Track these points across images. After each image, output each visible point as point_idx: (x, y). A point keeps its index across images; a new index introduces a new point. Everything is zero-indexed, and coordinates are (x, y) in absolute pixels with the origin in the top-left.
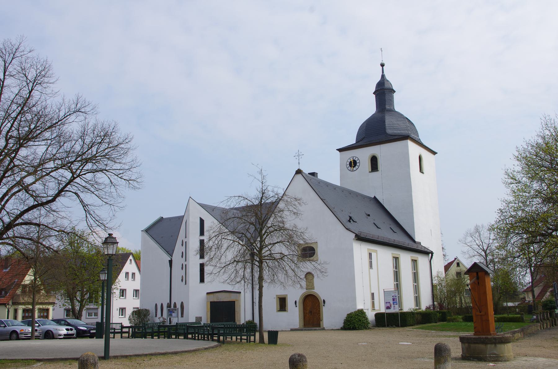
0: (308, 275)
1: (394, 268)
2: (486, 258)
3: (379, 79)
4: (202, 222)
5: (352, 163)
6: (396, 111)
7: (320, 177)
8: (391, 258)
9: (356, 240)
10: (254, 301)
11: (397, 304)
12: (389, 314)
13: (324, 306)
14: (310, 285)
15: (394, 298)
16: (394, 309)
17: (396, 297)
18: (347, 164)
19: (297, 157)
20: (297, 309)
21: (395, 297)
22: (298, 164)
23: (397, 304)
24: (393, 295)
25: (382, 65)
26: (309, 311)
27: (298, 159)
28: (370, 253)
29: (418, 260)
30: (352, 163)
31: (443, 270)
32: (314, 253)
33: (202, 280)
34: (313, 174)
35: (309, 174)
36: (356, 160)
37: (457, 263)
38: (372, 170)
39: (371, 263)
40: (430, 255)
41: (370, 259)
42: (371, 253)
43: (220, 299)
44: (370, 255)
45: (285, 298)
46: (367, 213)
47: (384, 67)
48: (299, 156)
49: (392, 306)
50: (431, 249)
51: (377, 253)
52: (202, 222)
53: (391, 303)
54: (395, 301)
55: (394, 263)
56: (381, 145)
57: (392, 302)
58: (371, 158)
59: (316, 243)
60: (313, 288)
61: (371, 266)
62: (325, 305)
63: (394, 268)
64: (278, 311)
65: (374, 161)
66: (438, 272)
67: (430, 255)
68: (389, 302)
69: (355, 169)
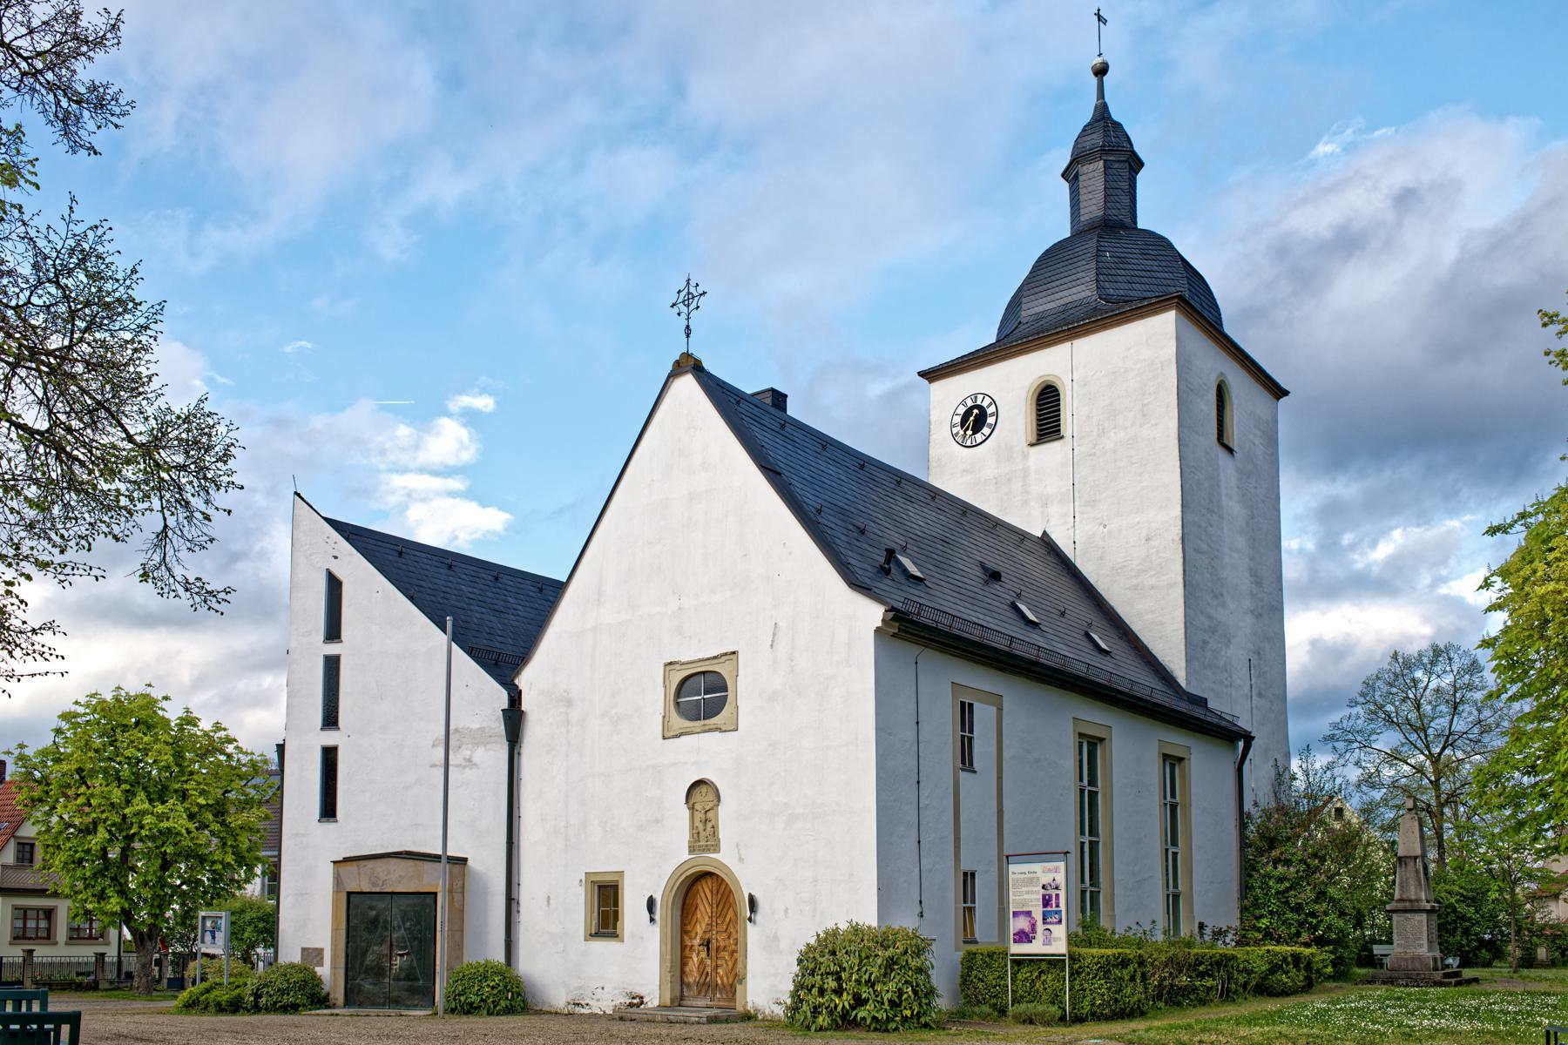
0: (696, 792)
1: (1081, 780)
2: (1437, 780)
3: (1087, 115)
4: (334, 586)
5: (972, 418)
8: (1071, 741)
9: (894, 635)
11: (1060, 922)
14: (704, 834)
16: (1047, 942)
17: (1057, 888)
18: (954, 421)
19: (684, 309)
20: (655, 931)
23: (1060, 922)
25: (1101, 71)
26: (701, 939)
27: (684, 316)
28: (963, 704)
29: (1189, 759)
30: (972, 418)
33: (329, 810)
38: (1038, 440)
41: (963, 729)
42: (971, 705)
43: (381, 883)
44: (966, 711)
46: (990, 565)
47: (1105, 78)
48: (690, 297)
49: (1040, 927)
50: (1244, 723)
51: (1000, 710)
52: (334, 586)
53: (1033, 915)
54: (1054, 909)
55: (1081, 761)
56: (1074, 342)
57: (1038, 914)
58: (1040, 389)
59: (732, 656)
60: (716, 848)
61: (966, 759)
63: (1081, 780)
64: (591, 935)
65: (1047, 402)
67: (1241, 744)
68: (1029, 914)
69: (979, 438)
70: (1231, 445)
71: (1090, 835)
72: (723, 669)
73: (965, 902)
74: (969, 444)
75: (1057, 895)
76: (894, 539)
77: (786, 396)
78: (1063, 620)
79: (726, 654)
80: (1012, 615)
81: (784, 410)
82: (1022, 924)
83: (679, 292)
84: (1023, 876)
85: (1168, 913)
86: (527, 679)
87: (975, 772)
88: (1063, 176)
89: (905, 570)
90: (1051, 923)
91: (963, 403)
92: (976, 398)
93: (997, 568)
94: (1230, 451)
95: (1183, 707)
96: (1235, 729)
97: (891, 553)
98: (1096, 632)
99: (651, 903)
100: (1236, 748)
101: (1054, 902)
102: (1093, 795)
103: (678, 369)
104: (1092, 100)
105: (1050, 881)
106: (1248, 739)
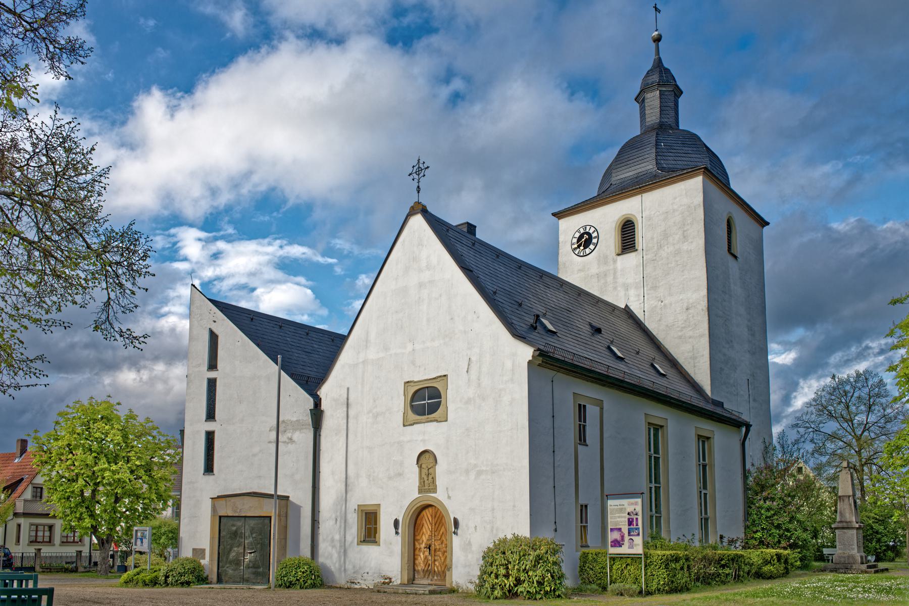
0: (423, 457)
1: (650, 450)
4: (213, 338)
11: (638, 535)
14: (427, 482)
16: (631, 547)
17: (636, 514)
19: (421, 166)
20: (399, 538)
21: (636, 516)
22: (416, 192)
23: (638, 535)
26: (425, 544)
27: (416, 181)
28: (580, 405)
32: (438, 405)
33: (209, 468)
36: (591, 232)
41: (580, 421)
42: (585, 406)
44: (582, 409)
45: (376, 513)
48: (420, 170)
49: (627, 538)
50: (745, 417)
52: (213, 338)
53: (623, 530)
54: (635, 527)
55: (585, 375)
57: (625, 530)
60: (434, 490)
61: (582, 438)
63: (650, 450)
67: (744, 429)
68: (620, 530)
70: (736, 254)
71: (655, 483)
75: (637, 519)
77: (475, 227)
78: (637, 356)
81: (474, 234)
82: (616, 536)
83: (413, 167)
84: (616, 507)
85: (702, 529)
86: (326, 391)
87: (587, 445)
89: (545, 327)
91: (578, 231)
92: (586, 228)
98: (657, 363)
99: (396, 523)
100: (740, 431)
101: (635, 523)
102: (657, 459)
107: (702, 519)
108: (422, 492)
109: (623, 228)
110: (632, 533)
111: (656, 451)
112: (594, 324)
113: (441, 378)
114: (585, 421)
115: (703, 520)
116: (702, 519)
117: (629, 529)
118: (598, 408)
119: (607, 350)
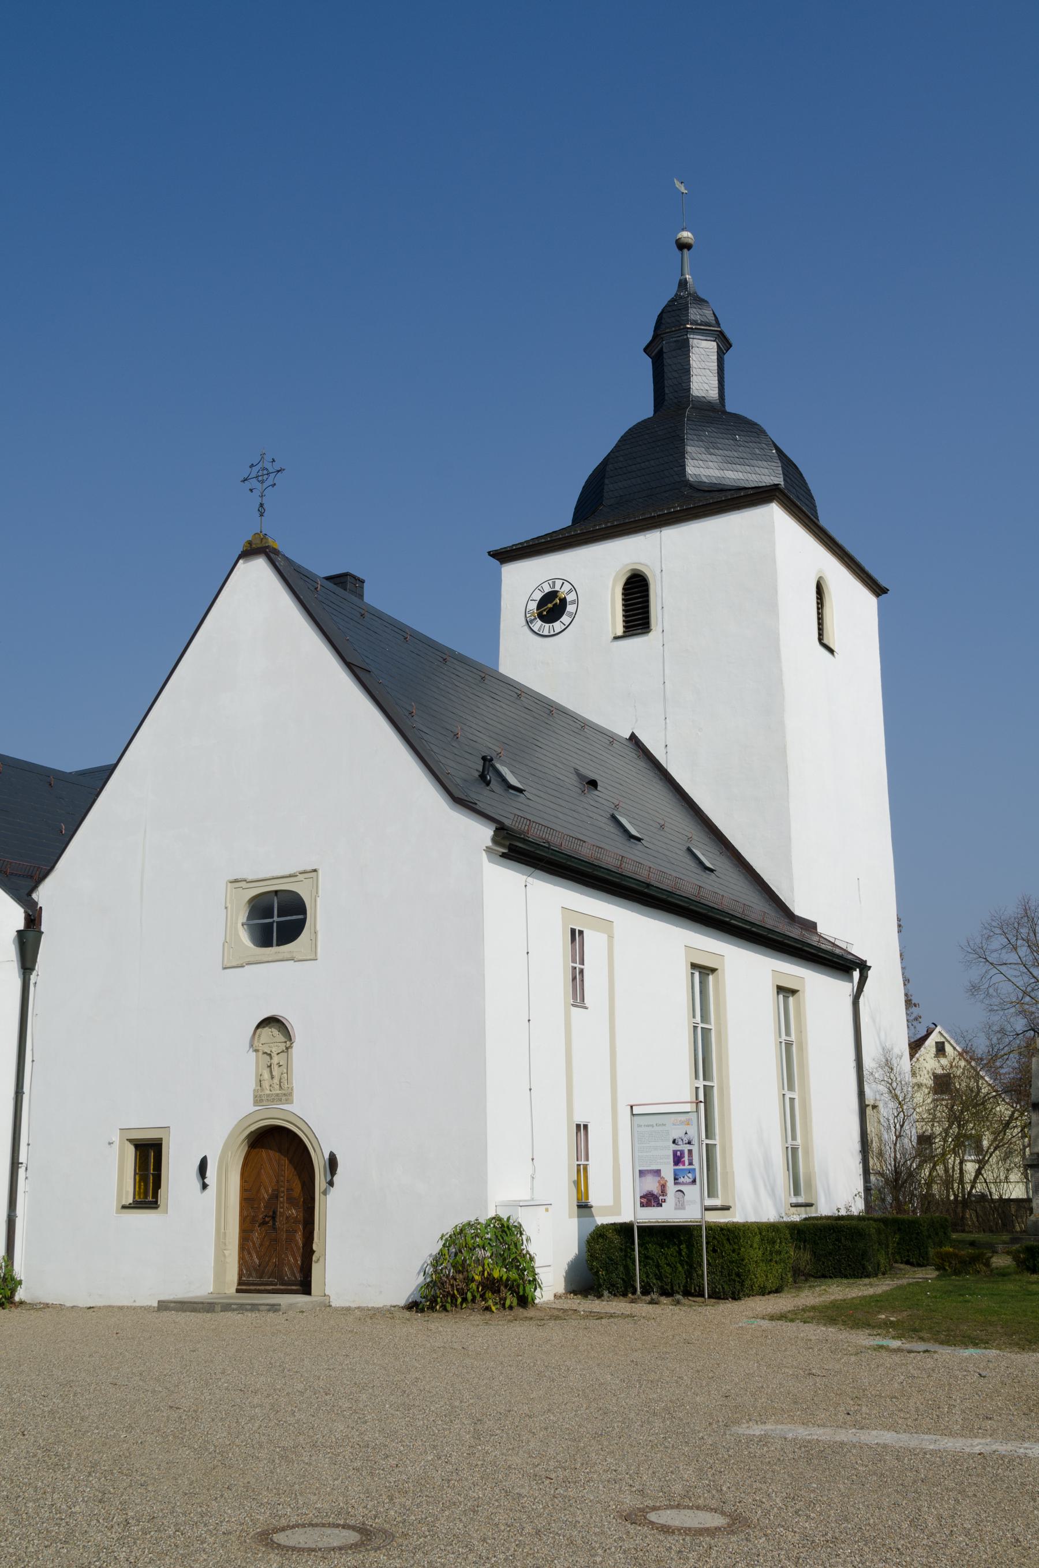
5: (550, 605)
6: (729, 413)
7: (372, 597)
9: (504, 856)
10: (22, 1158)
11: (694, 1182)
12: (652, 1233)
13: (331, 1183)
15: (682, 1152)
16: (680, 1206)
17: (689, 1143)
21: (688, 1147)
22: (258, 514)
23: (694, 1182)
24: (677, 1133)
27: (257, 493)
31: (903, 1046)
34: (341, 580)
35: (328, 578)
37: (937, 1043)
39: (577, 977)
40: (856, 974)
41: (574, 961)
42: (581, 932)
44: (576, 936)
49: (671, 1189)
50: (859, 951)
51: (611, 937)
53: (663, 1174)
54: (687, 1167)
57: (668, 1173)
60: (287, 1096)
62: (335, 1178)
63: (694, 1017)
64: (124, 1207)
66: (886, 1052)
67: (856, 974)
68: (657, 1172)
70: (832, 646)
71: (704, 1079)
72: (302, 890)
73: (577, 1160)
74: (536, 629)
75: (690, 1151)
76: (489, 745)
77: (363, 582)
78: (662, 833)
79: (305, 872)
80: (611, 828)
81: (361, 596)
83: (252, 466)
84: (650, 1128)
86: (43, 895)
87: (586, 1008)
88: (645, 350)
89: (504, 780)
90: (683, 1184)
91: (539, 587)
92: (554, 583)
93: (593, 776)
94: (831, 651)
95: (795, 932)
96: (850, 957)
97: (487, 761)
98: (697, 847)
100: (851, 980)
101: (686, 1159)
102: (706, 1032)
103: (249, 552)
104: (823, 522)
105: (682, 1135)
106: (864, 967)
107: (787, 1148)
108: (261, 1101)
109: (626, 584)
110: (681, 1180)
111: (705, 1018)
112: (583, 771)
113: (306, 875)
114: (582, 962)
115: (790, 1149)
116: (787, 1148)
117: (674, 1169)
118: (605, 936)
119: (609, 822)
